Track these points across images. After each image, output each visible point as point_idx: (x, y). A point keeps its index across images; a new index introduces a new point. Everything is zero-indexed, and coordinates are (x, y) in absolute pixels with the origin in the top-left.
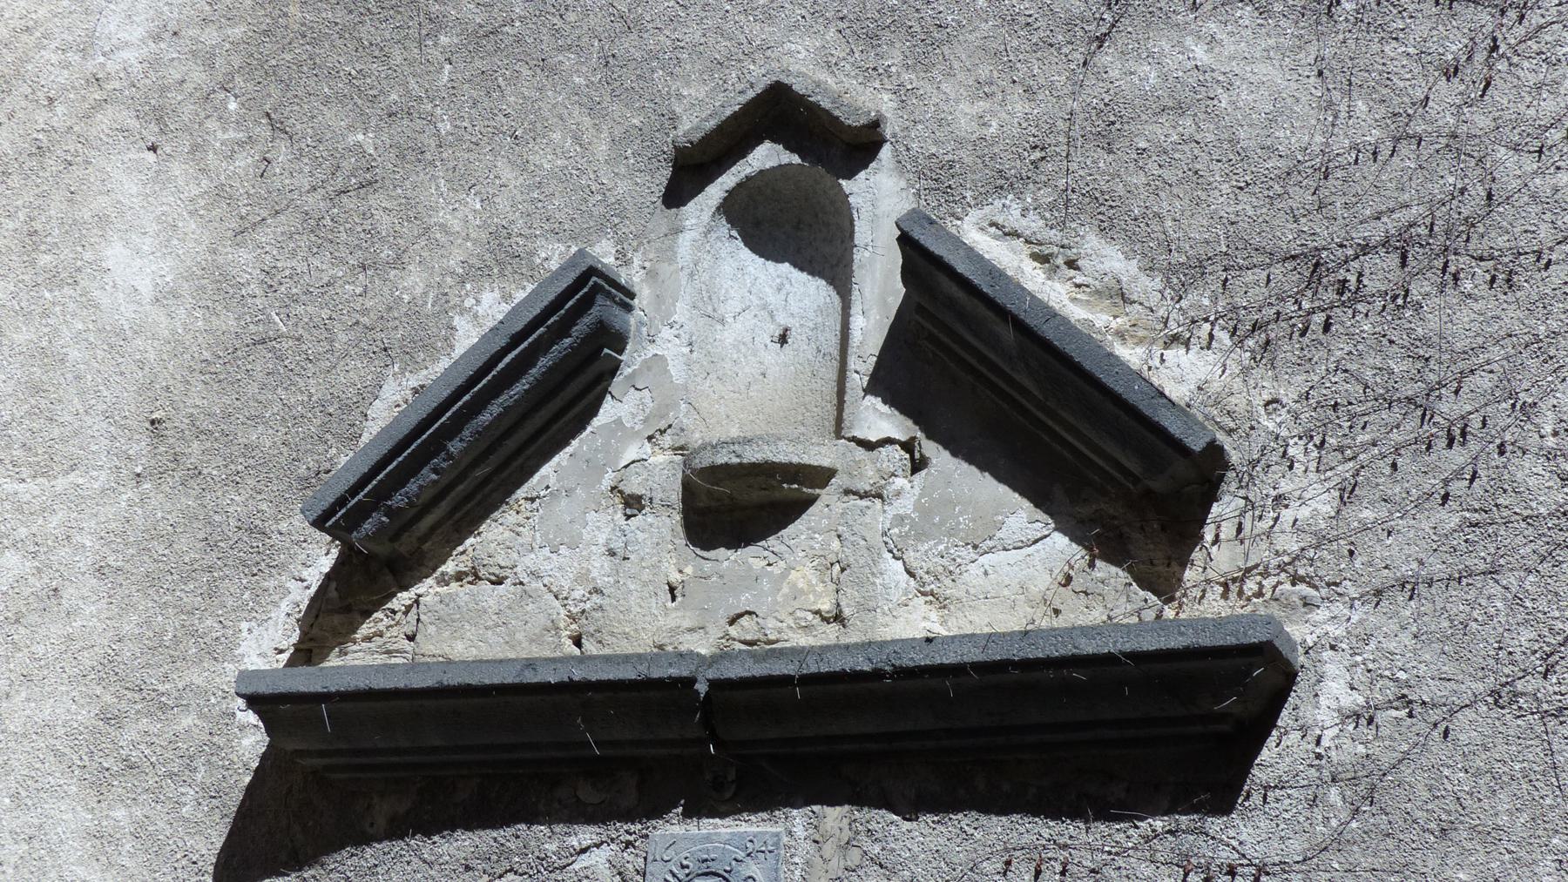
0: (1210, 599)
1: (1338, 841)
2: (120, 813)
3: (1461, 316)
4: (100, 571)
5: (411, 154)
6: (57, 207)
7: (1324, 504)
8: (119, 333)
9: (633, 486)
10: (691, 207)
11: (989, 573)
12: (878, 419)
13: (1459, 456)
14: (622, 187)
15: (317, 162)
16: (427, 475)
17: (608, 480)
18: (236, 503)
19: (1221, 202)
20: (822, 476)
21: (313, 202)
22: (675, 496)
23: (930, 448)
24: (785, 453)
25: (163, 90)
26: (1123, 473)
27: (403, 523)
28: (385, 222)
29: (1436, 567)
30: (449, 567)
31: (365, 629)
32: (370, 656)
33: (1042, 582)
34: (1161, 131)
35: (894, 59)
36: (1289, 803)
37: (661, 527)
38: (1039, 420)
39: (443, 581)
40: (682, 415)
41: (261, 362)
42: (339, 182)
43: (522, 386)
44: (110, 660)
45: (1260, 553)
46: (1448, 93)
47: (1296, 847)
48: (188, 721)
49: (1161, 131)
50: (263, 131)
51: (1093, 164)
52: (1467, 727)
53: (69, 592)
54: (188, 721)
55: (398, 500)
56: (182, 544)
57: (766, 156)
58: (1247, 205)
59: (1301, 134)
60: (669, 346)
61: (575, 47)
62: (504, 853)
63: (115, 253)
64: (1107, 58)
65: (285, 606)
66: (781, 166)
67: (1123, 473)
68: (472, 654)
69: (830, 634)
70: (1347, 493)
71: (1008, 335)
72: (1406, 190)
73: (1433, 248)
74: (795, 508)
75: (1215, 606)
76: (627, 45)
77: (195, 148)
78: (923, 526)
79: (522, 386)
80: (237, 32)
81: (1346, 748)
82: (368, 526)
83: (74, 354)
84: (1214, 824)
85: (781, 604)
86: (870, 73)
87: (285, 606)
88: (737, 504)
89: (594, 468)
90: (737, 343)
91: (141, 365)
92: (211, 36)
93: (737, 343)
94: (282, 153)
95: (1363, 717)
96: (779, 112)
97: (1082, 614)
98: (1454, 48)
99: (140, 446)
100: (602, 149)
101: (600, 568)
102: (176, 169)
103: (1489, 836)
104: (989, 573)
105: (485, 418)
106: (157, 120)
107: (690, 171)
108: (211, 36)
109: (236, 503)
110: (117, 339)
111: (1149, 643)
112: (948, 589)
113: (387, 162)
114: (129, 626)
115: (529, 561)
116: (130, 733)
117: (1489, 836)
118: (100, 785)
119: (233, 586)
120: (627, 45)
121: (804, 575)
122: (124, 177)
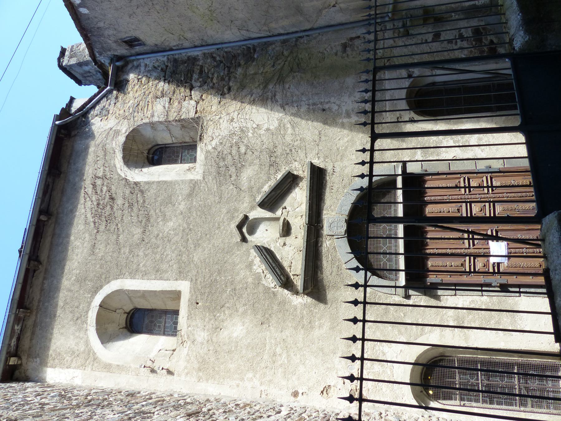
0: (304, 173)
1: (331, 160)
2: (317, 323)
3: (279, 151)
4: (282, 331)
5: (232, 283)
6: (225, 348)
7: (296, 163)
8: (247, 332)
9: (282, 244)
10: (249, 239)
11: (299, 198)
12: (279, 213)
13: (293, 150)
14: (244, 249)
15: (230, 299)
16: (277, 270)
17: (281, 248)
18: (275, 307)
19: (261, 175)
20: (285, 219)
21: (235, 299)
22: (284, 238)
23: (283, 206)
24: (281, 224)
25: (213, 328)
26: (289, 182)
27: (282, 274)
28: (241, 286)
29: (304, 152)
30: (289, 270)
31: (295, 283)
32: (299, 282)
33: (301, 192)
34: (252, 182)
35: (237, 214)
36: (327, 164)
37: (288, 240)
38: (269, 255)
39: (290, 271)
40: (275, 239)
41: (256, 305)
42: (233, 294)
43: (268, 257)
44: (295, 328)
45: (301, 169)
46: (255, 153)
47: (332, 164)
48: (305, 312)
49: (252, 182)
50: (223, 309)
51: (254, 190)
52: (321, 148)
53: (284, 337)
54: (305, 312)
55: (280, 274)
56: (280, 316)
57: (244, 230)
58: (263, 172)
59: (256, 167)
60: (265, 241)
61: (224, 258)
62: (326, 256)
63: (235, 335)
64: (243, 189)
65: (291, 297)
66: (246, 226)
67: (289, 182)
68: (301, 266)
69: (304, 217)
70: (295, 161)
71: (273, 193)
72: (265, 157)
73: (271, 153)
74: (288, 222)
75: (306, 173)
76: (226, 250)
77: (223, 321)
78: (292, 206)
79: (268, 257)
80: (207, 314)
81: (322, 159)
82: (282, 278)
83: (249, 341)
84: (328, 171)
85: (299, 224)
86: (238, 217)
87: (291, 297)
88: (287, 230)
89: (279, 250)
90: (267, 235)
91: (252, 327)
92: (207, 320)
93: (267, 235)
94: (227, 305)
95: (319, 158)
96: (240, 227)
97: (305, 187)
98: (251, 153)
99: (264, 326)
100: (238, 252)
101: (292, 248)
102: (225, 325)
103: (331, 146)
104: (299, 198)
105: (271, 261)
106: (217, 329)
107: (244, 239)
108: (207, 320)
109: (275, 307)
110: (248, 332)
111: (309, 179)
112: (300, 203)
113: (233, 287)
114: (290, 325)
115: (290, 258)
116: (305, 323)
117: (331, 146)
118: (312, 328)
119: (287, 307)
120: (226, 250)
121: (296, 220)
122: (224, 334)
